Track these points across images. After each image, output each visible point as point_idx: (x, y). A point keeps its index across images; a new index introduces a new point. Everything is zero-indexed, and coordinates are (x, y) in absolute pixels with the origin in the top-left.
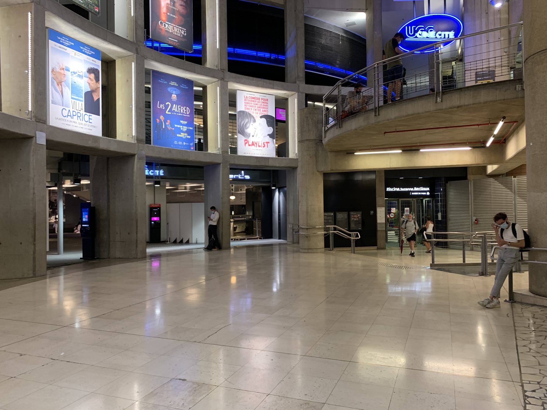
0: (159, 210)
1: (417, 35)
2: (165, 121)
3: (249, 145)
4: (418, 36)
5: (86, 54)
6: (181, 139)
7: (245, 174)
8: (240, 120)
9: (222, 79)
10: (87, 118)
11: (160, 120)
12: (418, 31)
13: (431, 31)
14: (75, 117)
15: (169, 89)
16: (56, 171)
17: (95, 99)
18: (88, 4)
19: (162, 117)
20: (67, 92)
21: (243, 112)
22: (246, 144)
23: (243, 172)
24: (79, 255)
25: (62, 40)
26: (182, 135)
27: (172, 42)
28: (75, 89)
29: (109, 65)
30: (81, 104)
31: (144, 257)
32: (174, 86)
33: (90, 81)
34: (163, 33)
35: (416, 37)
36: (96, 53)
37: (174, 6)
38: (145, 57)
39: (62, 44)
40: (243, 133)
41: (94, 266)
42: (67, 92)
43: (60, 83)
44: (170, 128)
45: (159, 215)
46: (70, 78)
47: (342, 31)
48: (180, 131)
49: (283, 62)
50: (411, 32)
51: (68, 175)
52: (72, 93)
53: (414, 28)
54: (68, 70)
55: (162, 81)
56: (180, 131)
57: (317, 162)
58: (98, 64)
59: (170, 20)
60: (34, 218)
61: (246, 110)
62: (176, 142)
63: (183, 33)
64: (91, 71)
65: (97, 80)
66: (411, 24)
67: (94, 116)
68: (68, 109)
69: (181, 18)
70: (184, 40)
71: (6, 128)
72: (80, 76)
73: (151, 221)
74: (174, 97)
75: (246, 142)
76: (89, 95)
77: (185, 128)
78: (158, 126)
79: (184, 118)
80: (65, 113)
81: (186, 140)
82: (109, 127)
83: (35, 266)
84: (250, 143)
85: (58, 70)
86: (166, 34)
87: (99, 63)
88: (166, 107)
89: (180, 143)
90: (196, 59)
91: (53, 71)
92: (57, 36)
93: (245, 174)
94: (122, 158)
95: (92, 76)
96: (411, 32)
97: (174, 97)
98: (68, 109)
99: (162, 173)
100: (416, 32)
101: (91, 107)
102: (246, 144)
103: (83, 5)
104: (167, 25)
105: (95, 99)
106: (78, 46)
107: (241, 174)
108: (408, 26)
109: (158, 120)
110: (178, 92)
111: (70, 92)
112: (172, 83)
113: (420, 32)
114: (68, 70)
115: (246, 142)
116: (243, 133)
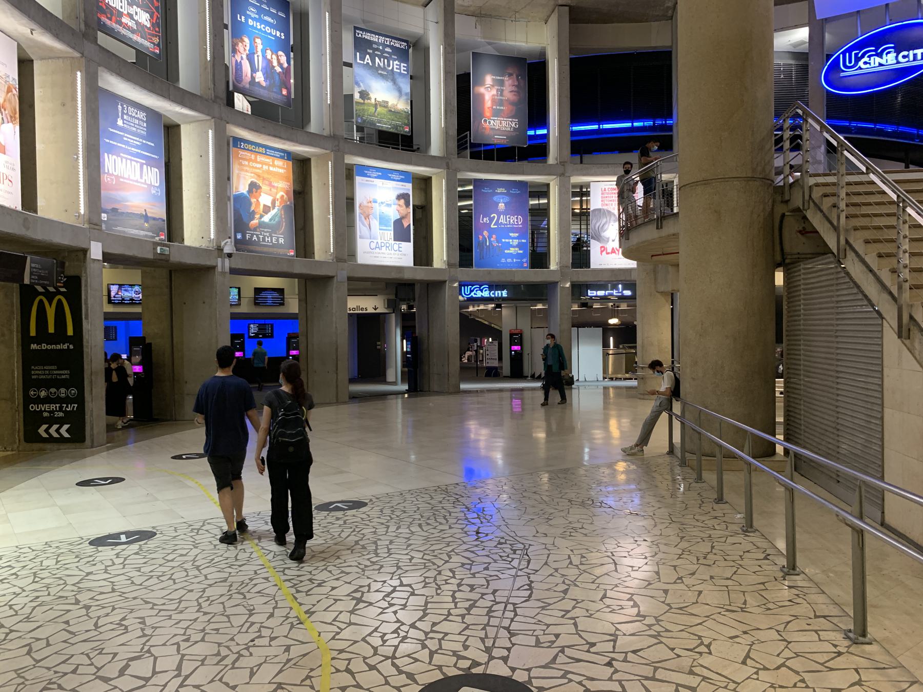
0: (521, 338)
1: (861, 64)
2: (490, 238)
3: (607, 253)
4: (863, 66)
5: (394, 180)
6: (511, 256)
7: (624, 289)
8: (594, 222)
9: (562, 175)
10: (396, 247)
11: (483, 236)
12: (863, 56)
13: (889, 53)
14: (384, 248)
15: (495, 198)
16: (393, 297)
17: (406, 225)
18: (396, 127)
19: (485, 233)
20: (375, 223)
21: (600, 210)
22: (602, 252)
23: (620, 286)
24: (405, 387)
25: (369, 173)
26: (512, 250)
27: (499, 139)
28: (383, 220)
29: (423, 185)
30: (390, 234)
31: (458, 392)
32: (501, 193)
33: (399, 208)
34: (487, 132)
35: (860, 68)
36: (406, 177)
37: (501, 95)
38: (457, 170)
39: (369, 177)
40: (598, 238)
41: (416, 396)
42: (375, 223)
43: (367, 217)
44: (495, 244)
45: (521, 343)
46: (378, 209)
47: (787, 55)
48: (509, 246)
49: (670, 128)
50: (850, 62)
51: (403, 300)
52: (380, 224)
53: (856, 55)
54: (375, 202)
55: (486, 190)
56: (509, 246)
57: (656, 279)
58: (408, 188)
59: (496, 113)
60: (337, 349)
61: (605, 207)
62: (503, 260)
63: (513, 125)
64: (403, 197)
65: (407, 204)
66: (850, 50)
67: (404, 244)
68: (375, 241)
69: (511, 107)
70: (514, 134)
71: (308, 272)
72: (389, 205)
73: (511, 351)
74: (502, 206)
75: (603, 249)
76: (398, 223)
77: (516, 242)
78: (481, 245)
79: (514, 230)
80: (373, 245)
81: (518, 256)
82: (423, 254)
83: (337, 393)
84: (609, 250)
85: (365, 203)
86: (492, 133)
87: (409, 186)
88: (491, 220)
89: (509, 260)
90: (536, 151)
91: (360, 206)
92: (364, 171)
93: (624, 289)
94: (434, 287)
95: (402, 201)
96: (850, 62)
97: (502, 206)
98: (375, 241)
99: (505, 293)
100: (858, 59)
101: (400, 234)
102: (602, 252)
103: (391, 130)
104: (492, 122)
105: (406, 225)
106: (385, 174)
107: (617, 289)
108: (844, 53)
109: (481, 237)
110: (507, 199)
111: (378, 223)
112: (499, 190)
113: (866, 59)
114: (375, 202)
115: (603, 249)
116: (598, 238)
